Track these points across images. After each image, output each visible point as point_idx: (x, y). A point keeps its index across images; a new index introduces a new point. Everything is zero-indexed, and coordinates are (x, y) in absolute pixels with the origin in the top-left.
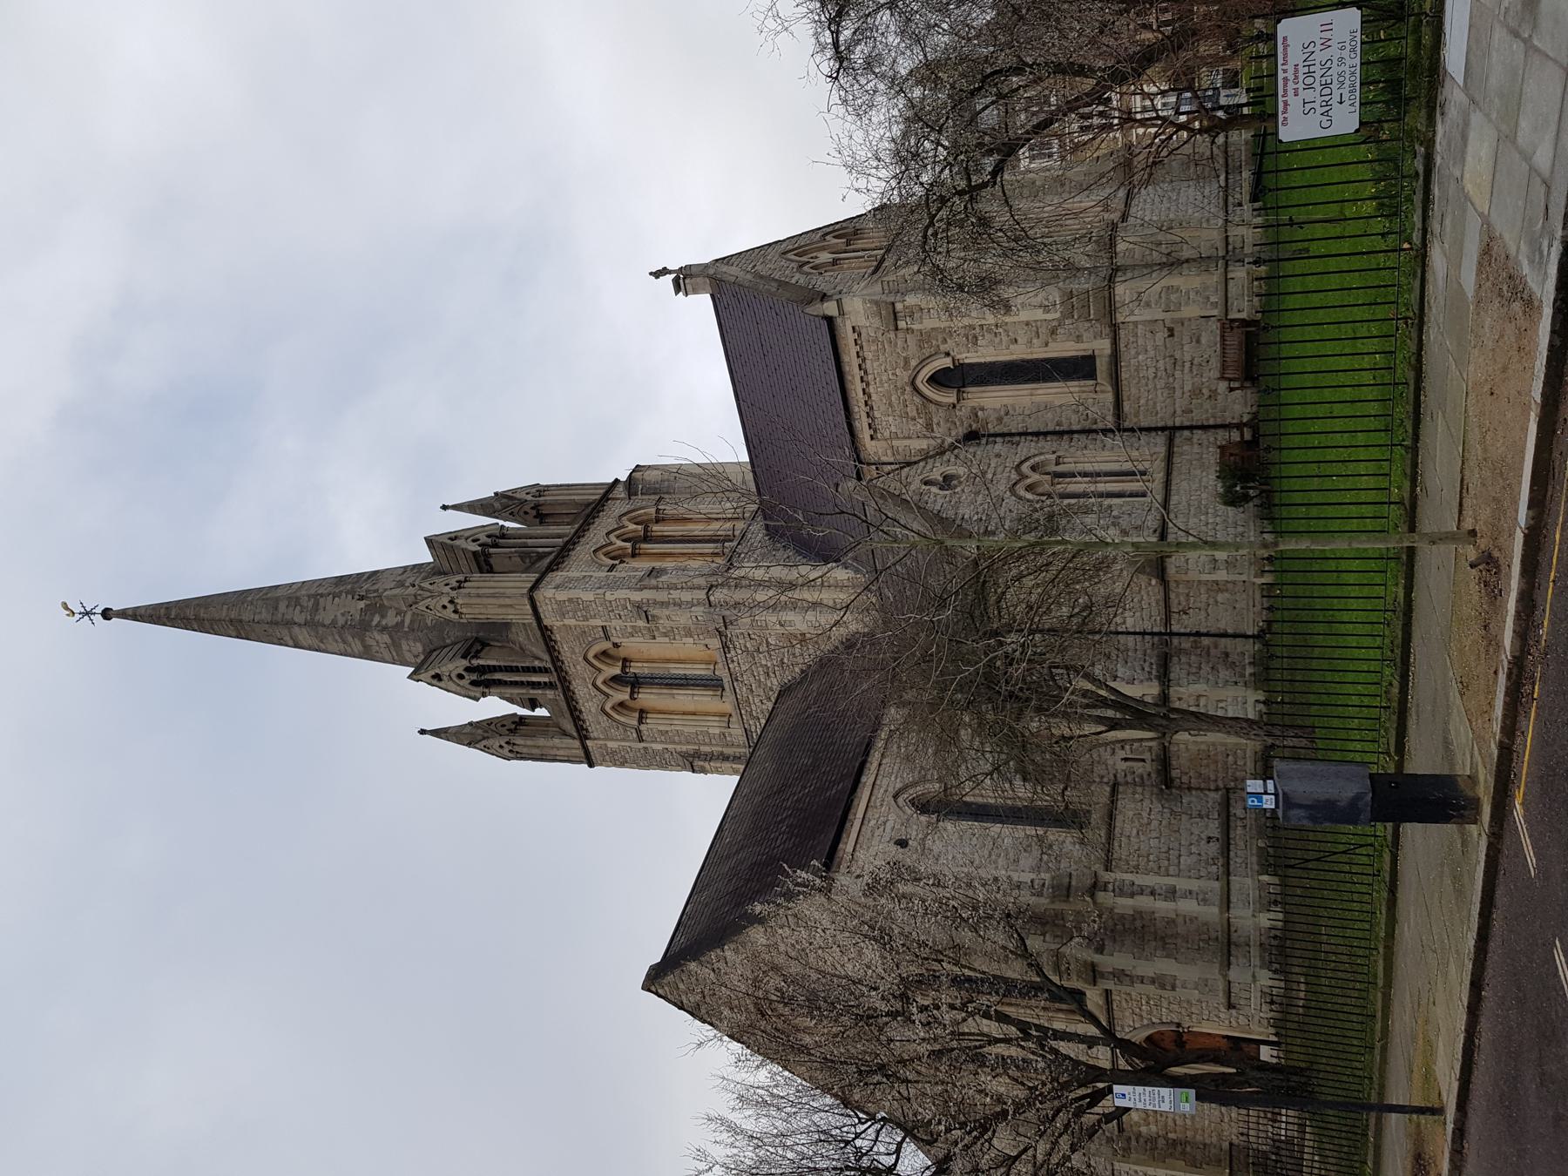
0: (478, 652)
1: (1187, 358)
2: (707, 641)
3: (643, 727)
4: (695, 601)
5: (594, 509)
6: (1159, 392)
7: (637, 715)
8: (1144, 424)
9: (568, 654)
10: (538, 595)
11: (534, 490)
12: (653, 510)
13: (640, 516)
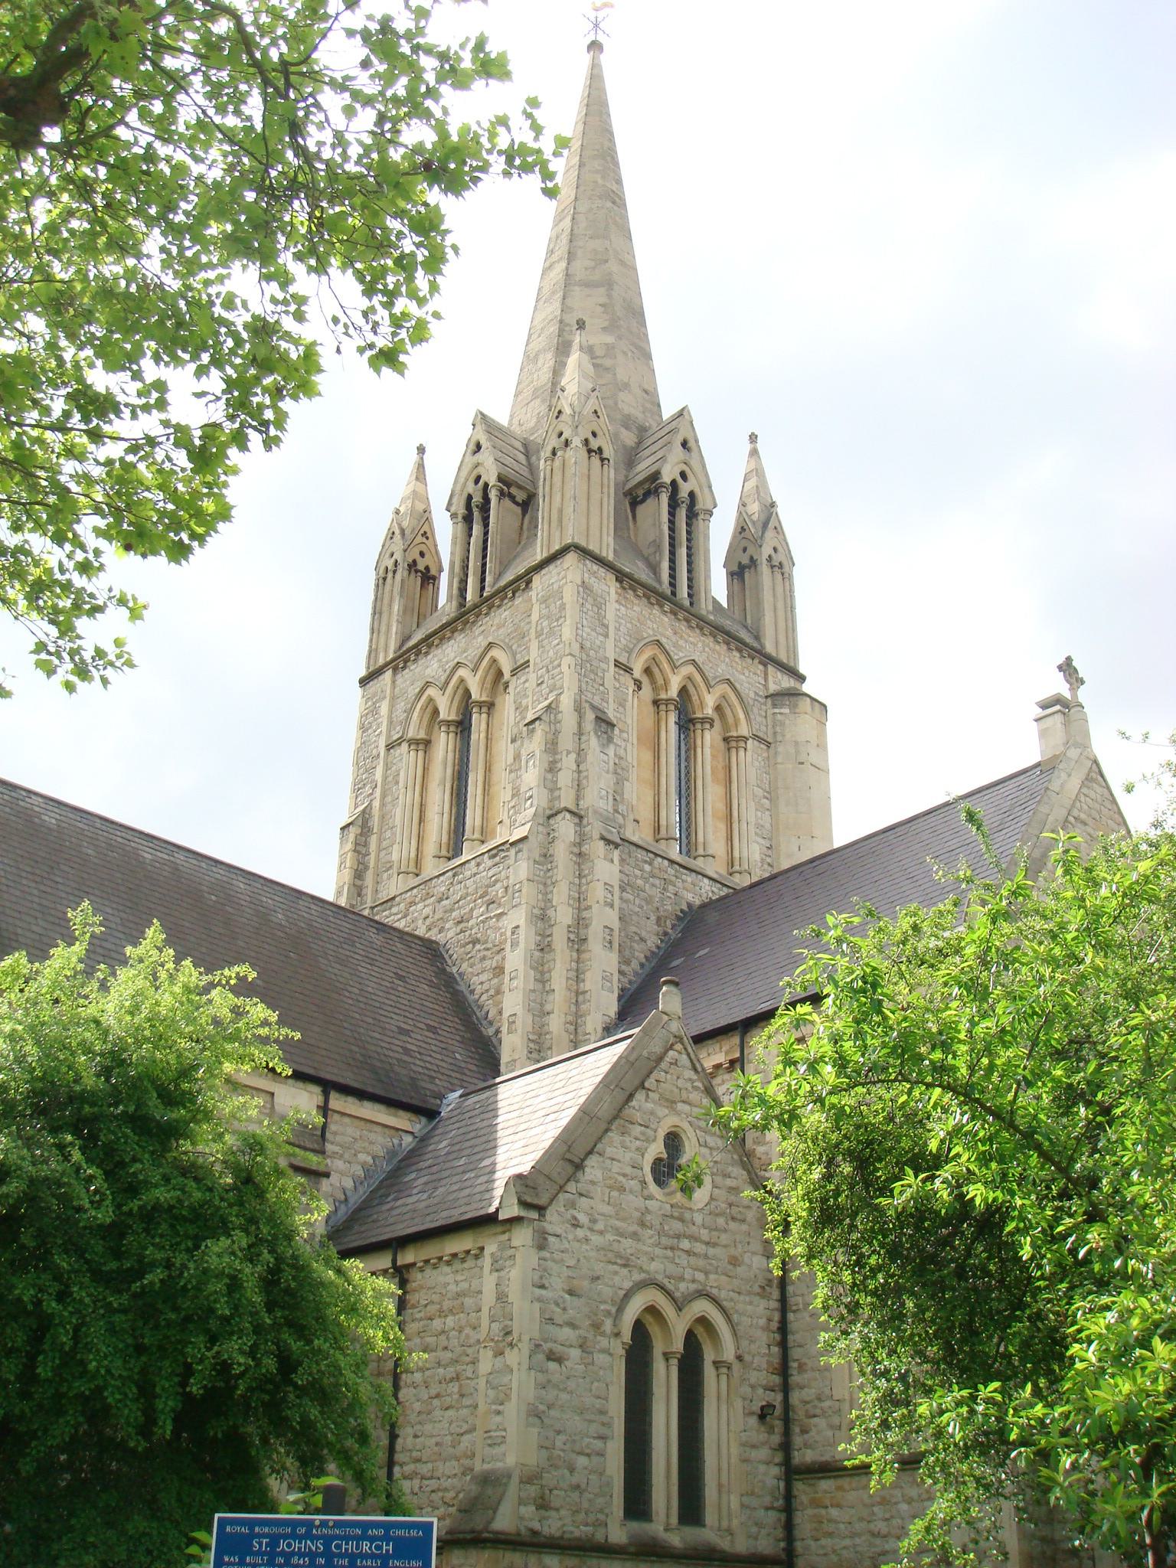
0: (512, 498)
3: (405, 746)
4: (557, 793)
5: (752, 648)
6: (847, 1542)
7: (422, 735)
8: (799, 1518)
9: (496, 621)
10: (571, 558)
12: (744, 730)
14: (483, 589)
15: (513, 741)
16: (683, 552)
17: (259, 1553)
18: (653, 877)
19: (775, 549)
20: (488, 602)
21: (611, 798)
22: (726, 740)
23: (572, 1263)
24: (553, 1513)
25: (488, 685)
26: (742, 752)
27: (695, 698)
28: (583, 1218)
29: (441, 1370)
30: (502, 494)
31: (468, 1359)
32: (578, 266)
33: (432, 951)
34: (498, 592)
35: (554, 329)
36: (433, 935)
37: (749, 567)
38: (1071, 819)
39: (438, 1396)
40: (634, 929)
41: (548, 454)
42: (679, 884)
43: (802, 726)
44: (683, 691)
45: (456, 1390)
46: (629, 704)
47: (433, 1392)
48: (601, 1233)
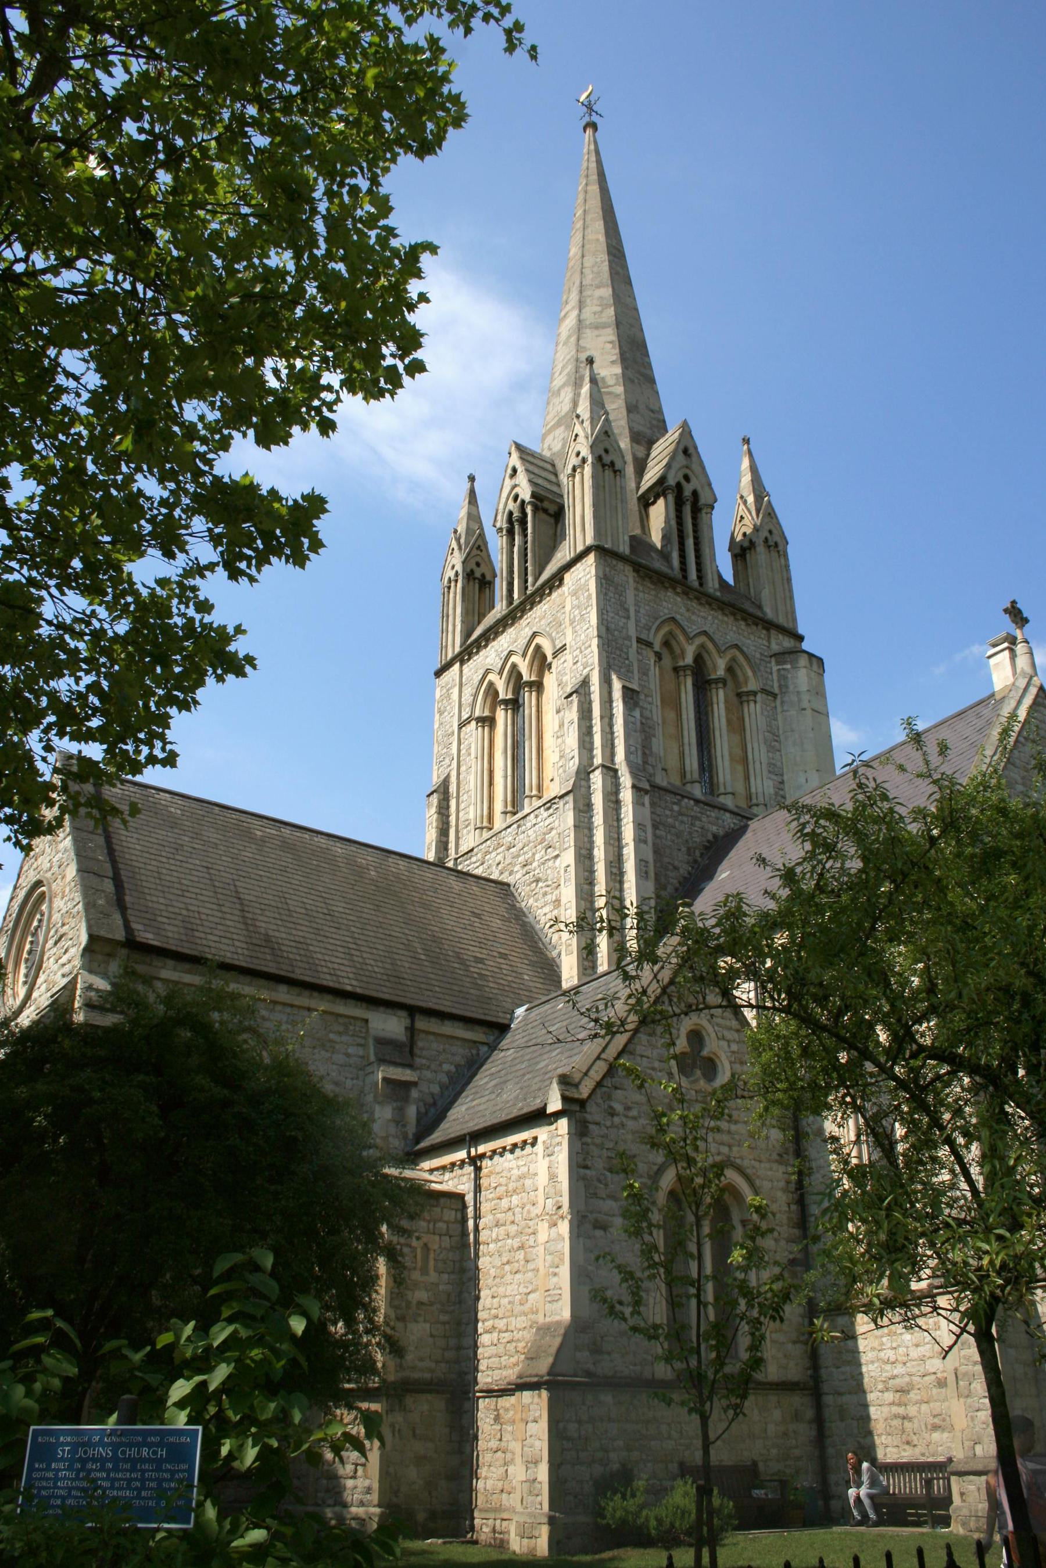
0: (545, 511)
1: (912, 1410)
2: (557, 780)
3: (473, 723)
7: (487, 713)
11: (777, 538)
12: (752, 685)
13: (741, 667)
14: (526, 588)
15: (558, 712)
16: (690, 542)
17: (62, 1459)
18: (682, 814)
19: (770, 532)
20: (530, 601)
21: (640, 753)
22: (739, 695)
23: (611, 1145)
24: (606, 1356)
25: (535, 668)
26: (752, 704)
27: (709, 663)
28: (618, 1107)
29: (509, 1241)
30: (536, 509)
31: (530, 1231)
32: (588, 314)
33: (504, 888)
34: (538, 590)
35: (570, 367)
36: (505, 878)
37: (750, 549)
38: (1021, 739)
39: (508, 1262)
40: (666, 860)
41: (569, 471)
42: (704, 819)
43: (802, 677)
44: (698, 659)
45: (522, 1257)
46: (651, 673)
47: (505, 1260)
48: (634, 1118)
